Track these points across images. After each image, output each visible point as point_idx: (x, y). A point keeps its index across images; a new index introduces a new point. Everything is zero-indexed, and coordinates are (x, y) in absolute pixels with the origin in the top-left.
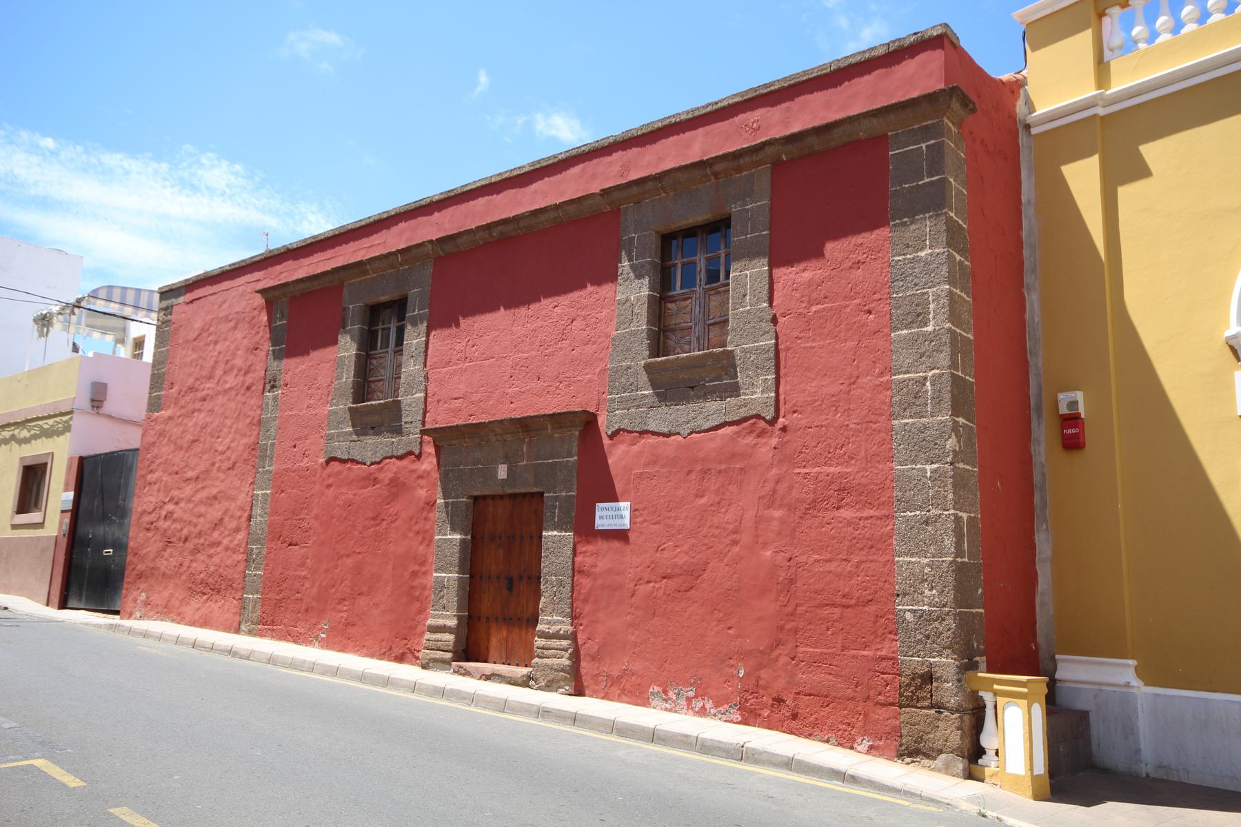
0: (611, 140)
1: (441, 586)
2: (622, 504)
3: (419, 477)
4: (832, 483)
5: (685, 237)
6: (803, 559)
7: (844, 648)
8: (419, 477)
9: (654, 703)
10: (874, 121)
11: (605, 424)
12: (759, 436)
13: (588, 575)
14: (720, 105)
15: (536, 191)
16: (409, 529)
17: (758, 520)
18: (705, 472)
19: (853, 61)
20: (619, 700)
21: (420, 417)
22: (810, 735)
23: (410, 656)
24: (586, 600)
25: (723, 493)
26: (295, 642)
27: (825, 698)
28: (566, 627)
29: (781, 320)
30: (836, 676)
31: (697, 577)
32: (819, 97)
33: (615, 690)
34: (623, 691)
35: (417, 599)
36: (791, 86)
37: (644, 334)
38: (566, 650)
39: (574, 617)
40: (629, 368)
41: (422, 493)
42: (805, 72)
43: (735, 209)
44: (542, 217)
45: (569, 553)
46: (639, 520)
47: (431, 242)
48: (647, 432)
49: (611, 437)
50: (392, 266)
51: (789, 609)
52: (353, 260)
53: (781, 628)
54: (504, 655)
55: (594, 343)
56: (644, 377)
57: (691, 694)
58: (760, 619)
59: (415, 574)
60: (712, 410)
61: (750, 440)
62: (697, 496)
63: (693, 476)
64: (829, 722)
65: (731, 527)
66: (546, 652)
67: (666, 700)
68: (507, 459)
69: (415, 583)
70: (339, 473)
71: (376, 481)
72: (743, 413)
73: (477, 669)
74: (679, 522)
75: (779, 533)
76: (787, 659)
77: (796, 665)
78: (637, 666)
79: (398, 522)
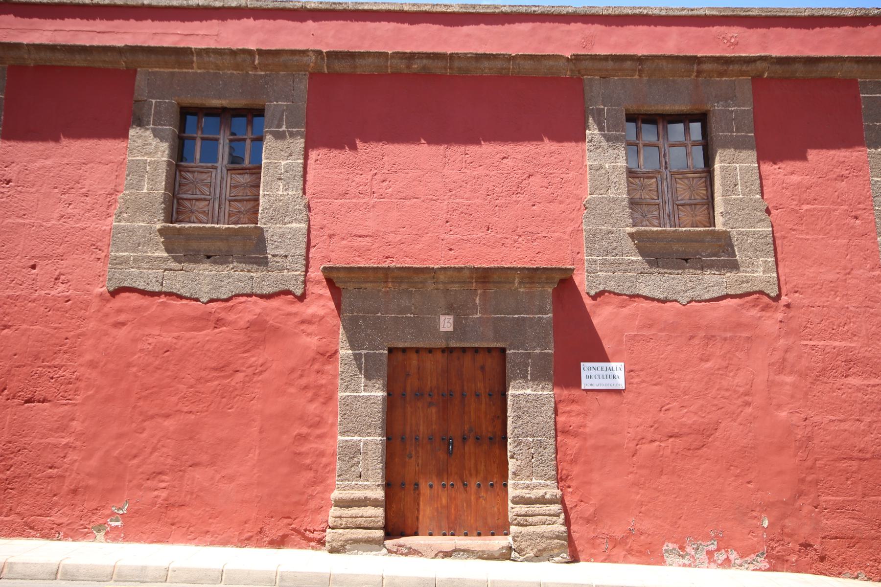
0: (571, 10)
1: (355, 451)
2: (613, 364)
3: (303, 322)
4: (838, 355)
5: (645, 121)
6: (818, 419)
7: (864, 495)
8: (303, 322)
9: (668, 560)
10: (856, 66)
11: (583, 282)
12: (763, 310)
13: (575, 435)
14: (695, 13)
15: (468, 35)
16: (290, 384)
17: (771, 384)
18: (709, 338)
19: (826, 13)
20: (625, 560)
21: (303, 252)
22: (840, 573)
23: (297, 538)
24: (574, 461)
25: (730, 359)
26: (45, 536)
27: (851, 540)
28: (552, 491)
29: (773, 212)
30: (859, 519)
31: (709, 436)
32: (793, 34)
33: (619, 551)
34: (630, 551)
35: (309, 468)
36: (767, 17)
37: (625, 203)
38: (557, 515)
39: (560, 479)
40: (610, 232)
41: (312, 342)
42: (781, 10)
43: (718, 107)
44: (486, 64)
45: (550, 412)
46: (636, 380)
47: (319, 52)
48: (638, 296)
49: (594, 298)
50: (237, 67)
51: (809, 463)
52: (153, 43)
53: (803, 481)
54: (444, 524)
55: (561, 202)
56: (630, 244)
57: (713, 547)
58: (780, 473)
59: (302, 438)
60: (712, 282)
61: (755, 312)
62: (702, 360)
63: (696, 341)
64: (857, 560)
65: (741, 390)
66: (530, 519)
67: (683, 557)
68: (450, 309)
69: (304, 449)
70: (137, 310)
71: (219, 322)
72: (746, 288)
73: (430, 546)
74: (683, 384)
75: (792, 397)
76: (810, 507)
77: (820, 513)
78: (647, 525)
79: (265, 375)
